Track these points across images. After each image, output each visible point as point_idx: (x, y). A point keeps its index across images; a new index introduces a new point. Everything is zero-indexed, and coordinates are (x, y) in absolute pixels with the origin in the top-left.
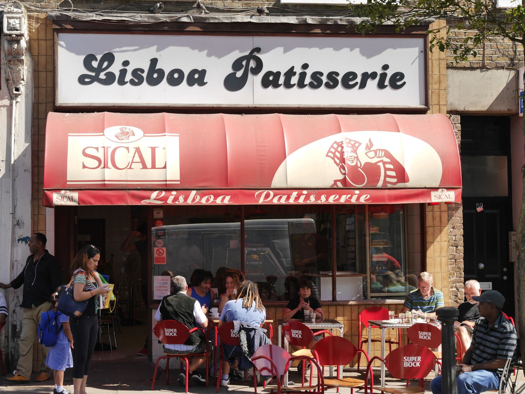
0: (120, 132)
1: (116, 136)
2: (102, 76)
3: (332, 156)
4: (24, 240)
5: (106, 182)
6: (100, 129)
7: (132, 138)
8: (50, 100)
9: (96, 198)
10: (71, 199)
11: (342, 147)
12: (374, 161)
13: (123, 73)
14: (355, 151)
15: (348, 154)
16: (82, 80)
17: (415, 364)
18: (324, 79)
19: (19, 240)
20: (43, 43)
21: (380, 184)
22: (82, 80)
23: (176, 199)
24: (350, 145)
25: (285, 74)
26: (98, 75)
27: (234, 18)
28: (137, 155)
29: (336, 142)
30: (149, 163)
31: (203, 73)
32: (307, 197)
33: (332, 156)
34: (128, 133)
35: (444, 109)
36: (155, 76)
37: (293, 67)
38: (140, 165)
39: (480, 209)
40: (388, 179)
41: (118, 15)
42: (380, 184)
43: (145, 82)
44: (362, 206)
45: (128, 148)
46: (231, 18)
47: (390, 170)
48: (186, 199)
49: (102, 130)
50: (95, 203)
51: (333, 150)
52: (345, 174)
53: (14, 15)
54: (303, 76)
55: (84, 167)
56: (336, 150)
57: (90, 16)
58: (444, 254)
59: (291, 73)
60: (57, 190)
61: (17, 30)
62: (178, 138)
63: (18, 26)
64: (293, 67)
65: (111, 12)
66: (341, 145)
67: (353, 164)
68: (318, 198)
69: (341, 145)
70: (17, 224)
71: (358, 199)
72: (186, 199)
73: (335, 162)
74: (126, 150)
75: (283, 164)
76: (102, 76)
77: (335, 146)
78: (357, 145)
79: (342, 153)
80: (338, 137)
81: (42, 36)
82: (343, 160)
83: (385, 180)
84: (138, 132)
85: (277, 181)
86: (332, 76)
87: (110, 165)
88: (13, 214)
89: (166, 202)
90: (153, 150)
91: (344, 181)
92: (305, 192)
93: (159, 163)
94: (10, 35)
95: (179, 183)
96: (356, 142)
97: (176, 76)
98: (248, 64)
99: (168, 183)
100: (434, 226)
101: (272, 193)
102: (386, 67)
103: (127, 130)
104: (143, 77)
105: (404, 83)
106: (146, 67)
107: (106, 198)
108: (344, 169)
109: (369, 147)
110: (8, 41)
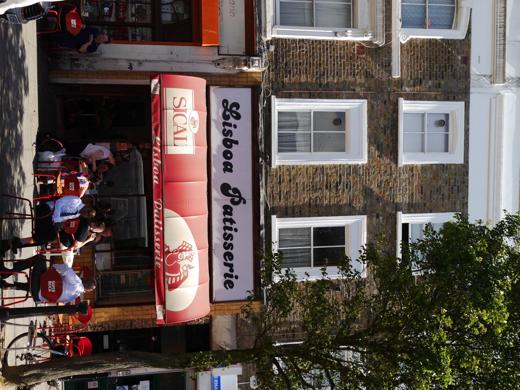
0: (196, 120)
1: (192, 118)
2: (228, 113)
3: (184, 245)
4: (131, 67)
5: (165, 111)
6: (197, 108)
7: (192, 126)
8: (213, 84)
9: (156, 105)
10: (155, 89)
11: (189, 251)
12: (181, 270)
13: (230, 125)
14: (186, 258)
15: (185, 254)
16: (225, 101)
17: (50, 288)
18: (229, 242)
19: (130, 63)
20: (245, 80)
21: (167, 274)
22: (225, 101)
23: (156, 152)
24: (190, 255)
25: (231, 218)
26: (228, 110)
27: (262, 188)
28: (182, 129)
29: (192, 247)
30: (177, 136)
31: (231, 171)
32: (158, 230)
33: (184, 245)
34: (195, 124)
35: (213, 314)
36: (229, 143)
37: (235, 223)
38: (176, 131)
39: (153, 338)
40: (170, 279)
41: (262, 122)
42: (167, 274)
43: (225, 137)
44: (153, 263)
45: (186, 124)
46: (262, 186)
47: (176, 280)
48: (156, 157)
49: (196, 109)
50: (153, 103)
51: (187, 245)
52: (173, 252)
53: (260, 63)
54: (230, 229)
55: (174, 98)
56: (187, 247)
57: (261, 106)
58: (125, 318)
59: (232, 222)
60: (160, 82)
61: (252, 65)
62: (193, 153)
63: (255, 65)
64: (235, 223)
65: (263, 119)
66: (190, 250)
67: (179, 257)
68: (158, 236)
69: (190, 250)
70: (140, 63)
71: (158, 261)
72: (156, 157)
73: (180, 247)
74: (185, 123)
75: (179, 215)
76: (228, 113)
77: (190, 246)
78: (190, 259)
79: (185, 251)
80: (195, 247)
81: (249, 79)
82: (181, 251)
83: (169, 277)
84: (196, 130)
85: (167, 212)
86: (231, 246)
87: (176, 113)
88: (146, 61)
89: (154, 146)
90: (185, 139)
91: (169, 252)
92: (161, 229)
93: (177, 142)
94: (249, 61)
95: (166, 153)
96: (192, 259)
97: (229, 155)
98: (236, 197)
99: (166, 147)
100: (142, 310)
101: (161, 208)
102: (237, 277)
103: (196, 124)
104: (227, 136)
105: (227, 289)
106: (233, 138)
107: (156, 110)
108: (176, 252)
109: (189, 267)
110: (246, 60)
